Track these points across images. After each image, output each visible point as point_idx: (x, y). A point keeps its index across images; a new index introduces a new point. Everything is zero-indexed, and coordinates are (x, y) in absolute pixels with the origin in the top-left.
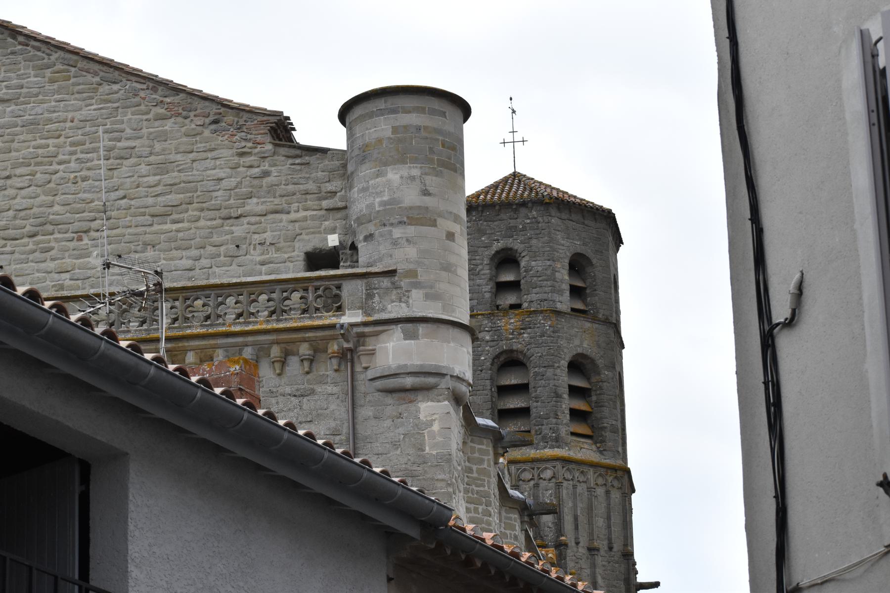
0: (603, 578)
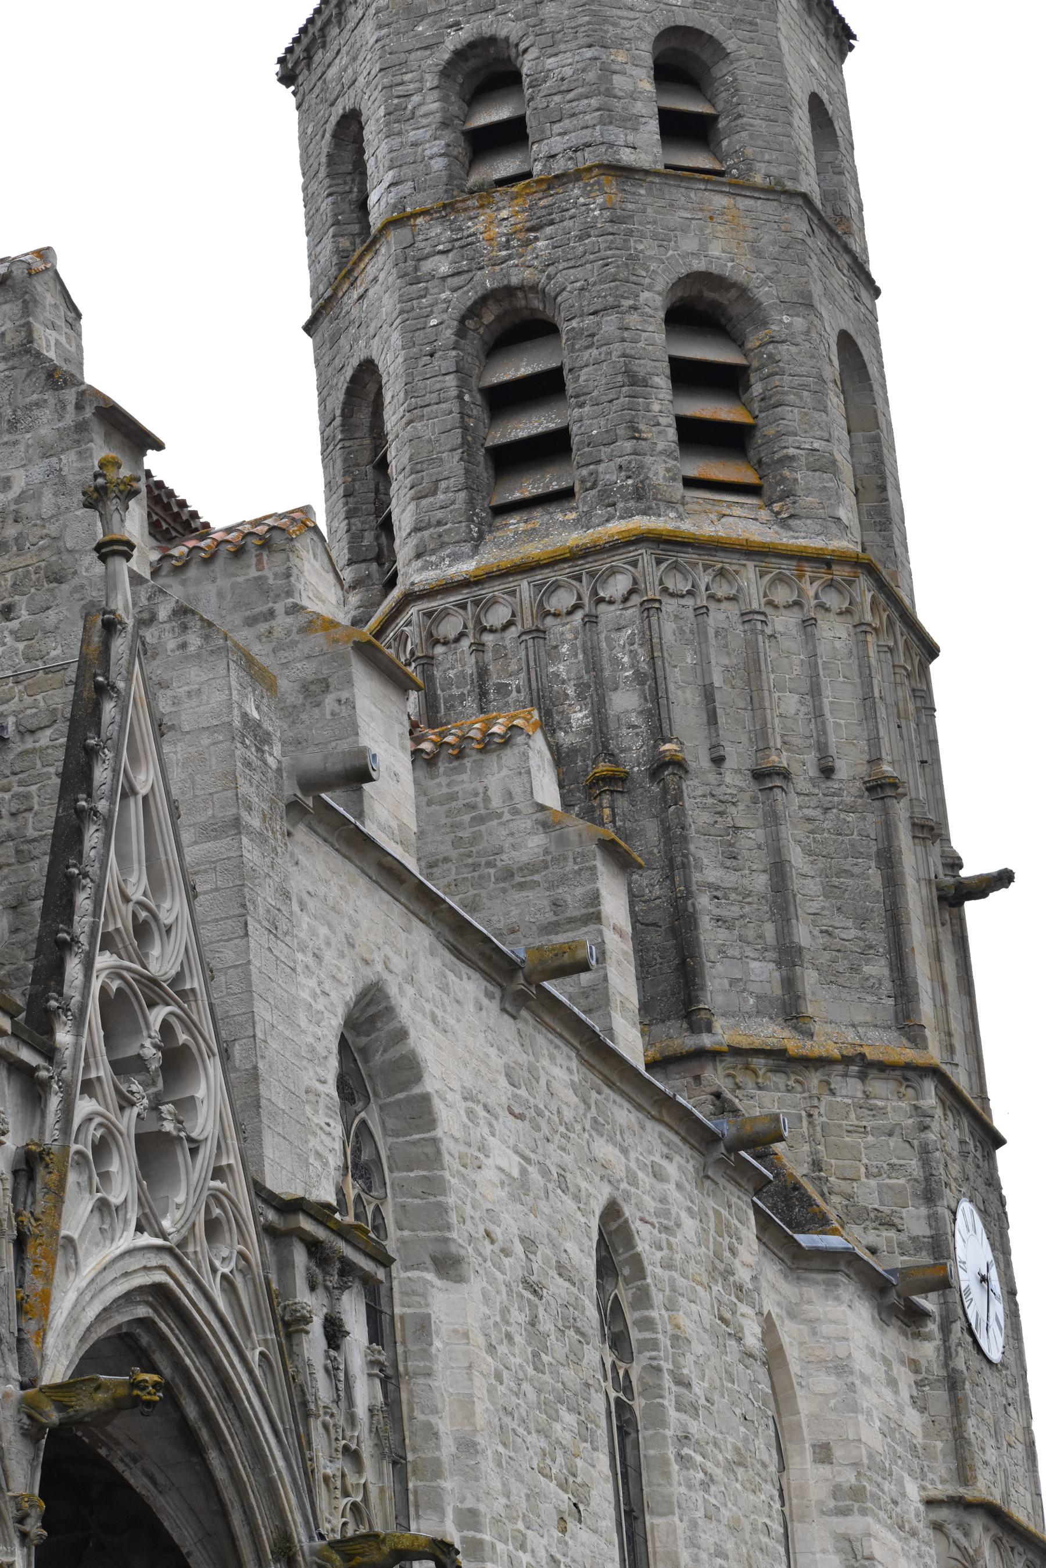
0: (809, 853)
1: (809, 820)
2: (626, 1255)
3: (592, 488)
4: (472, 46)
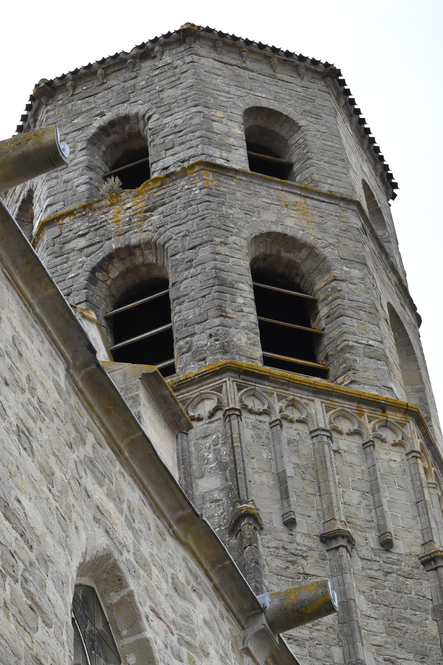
1: (371, 578)
2: (132, 639)
3: (187, 352)
4: (112, 124)
